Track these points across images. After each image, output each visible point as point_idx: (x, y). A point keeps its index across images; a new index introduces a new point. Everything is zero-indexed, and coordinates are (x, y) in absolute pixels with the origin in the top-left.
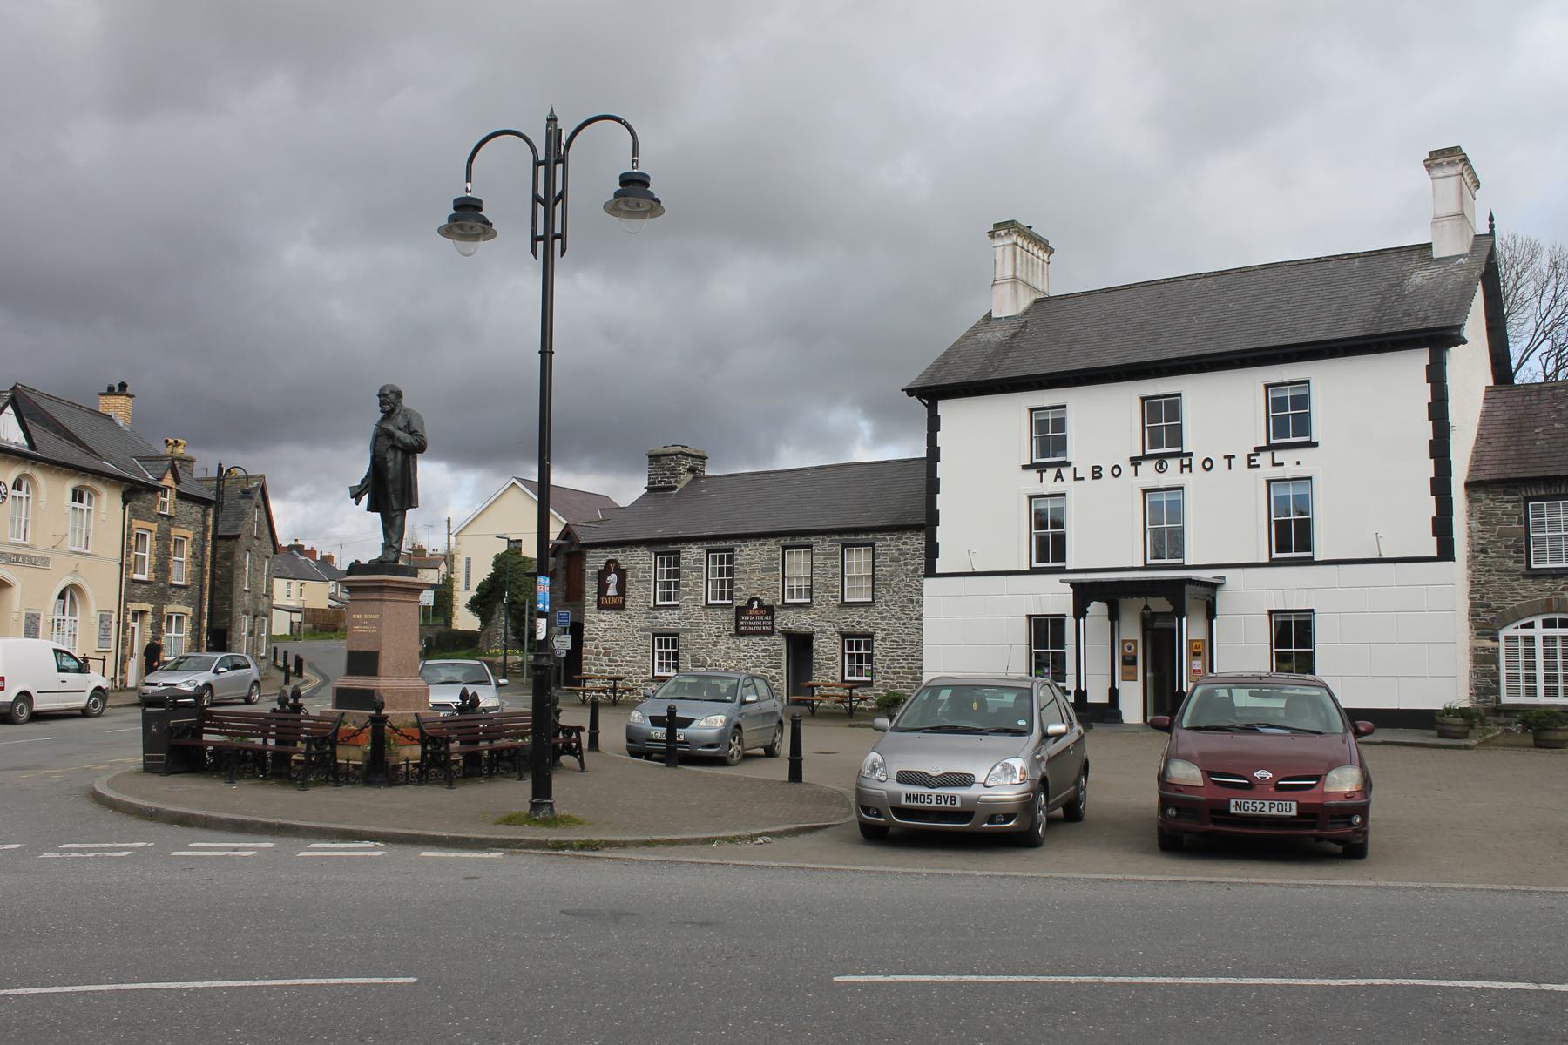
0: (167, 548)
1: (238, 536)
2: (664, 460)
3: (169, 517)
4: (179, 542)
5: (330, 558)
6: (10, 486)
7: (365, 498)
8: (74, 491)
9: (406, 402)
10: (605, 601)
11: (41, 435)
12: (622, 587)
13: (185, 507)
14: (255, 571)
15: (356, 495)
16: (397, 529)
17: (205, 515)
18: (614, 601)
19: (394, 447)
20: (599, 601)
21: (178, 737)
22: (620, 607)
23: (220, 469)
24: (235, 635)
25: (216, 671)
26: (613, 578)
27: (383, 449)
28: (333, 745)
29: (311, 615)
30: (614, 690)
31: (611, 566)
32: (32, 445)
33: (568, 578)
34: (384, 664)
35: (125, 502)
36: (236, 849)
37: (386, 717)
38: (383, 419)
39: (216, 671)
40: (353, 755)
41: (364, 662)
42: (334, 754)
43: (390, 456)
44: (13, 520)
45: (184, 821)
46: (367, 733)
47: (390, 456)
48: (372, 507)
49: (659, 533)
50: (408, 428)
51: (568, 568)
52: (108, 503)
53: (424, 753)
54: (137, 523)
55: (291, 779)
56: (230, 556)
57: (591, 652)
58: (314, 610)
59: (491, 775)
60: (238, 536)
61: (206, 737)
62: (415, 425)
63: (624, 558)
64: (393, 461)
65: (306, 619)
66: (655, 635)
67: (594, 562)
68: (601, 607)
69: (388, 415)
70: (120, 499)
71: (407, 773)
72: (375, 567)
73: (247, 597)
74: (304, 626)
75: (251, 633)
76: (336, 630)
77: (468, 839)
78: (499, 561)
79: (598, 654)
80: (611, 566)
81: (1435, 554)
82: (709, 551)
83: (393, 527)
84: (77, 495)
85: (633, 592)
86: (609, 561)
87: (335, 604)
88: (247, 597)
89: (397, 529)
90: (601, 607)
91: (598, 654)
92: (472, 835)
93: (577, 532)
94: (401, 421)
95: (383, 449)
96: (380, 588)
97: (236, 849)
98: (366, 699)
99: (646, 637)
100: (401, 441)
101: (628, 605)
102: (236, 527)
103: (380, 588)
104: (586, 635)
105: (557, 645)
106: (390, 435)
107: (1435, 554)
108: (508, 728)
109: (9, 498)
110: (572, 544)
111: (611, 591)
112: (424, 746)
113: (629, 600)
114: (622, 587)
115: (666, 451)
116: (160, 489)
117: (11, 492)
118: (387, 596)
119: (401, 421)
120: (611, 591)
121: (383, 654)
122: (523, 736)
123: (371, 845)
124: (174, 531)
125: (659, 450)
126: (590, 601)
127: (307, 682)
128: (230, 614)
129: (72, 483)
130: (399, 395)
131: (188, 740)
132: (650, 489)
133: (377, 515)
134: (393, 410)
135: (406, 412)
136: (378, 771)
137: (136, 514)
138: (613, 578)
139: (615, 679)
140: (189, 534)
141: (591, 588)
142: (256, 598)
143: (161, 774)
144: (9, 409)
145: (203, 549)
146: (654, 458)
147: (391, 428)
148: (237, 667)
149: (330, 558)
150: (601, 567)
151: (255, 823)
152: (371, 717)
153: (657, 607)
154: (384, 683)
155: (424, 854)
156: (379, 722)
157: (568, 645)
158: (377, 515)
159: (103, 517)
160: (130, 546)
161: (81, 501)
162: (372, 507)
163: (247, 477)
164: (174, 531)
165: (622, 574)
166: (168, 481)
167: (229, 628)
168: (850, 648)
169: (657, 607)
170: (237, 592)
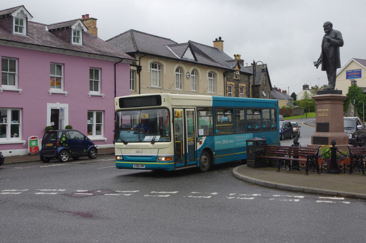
0: (238, 90)
3: (238, 80)
4: (242, 89)
6: (191, 73)
7: (320, 66)
8: (209, 73)
9: (334, 28)
11: (198, 57)
13: (243, 76)
17: (249, 79)
32: (196, 60)
34: (331, 127)
35: (224, 76)
38: (326, 35)
44: (192, 84)
45: (276, 188)
48: (323, 69)
52: (220, 77)
54: (228, 83)
60: (260, 85)
70: (223, 75)
71: (322, 168)
72: (326, 90)
78: (350, 89)
81: (185, 109)
83: (332, 77)
84: (210, 75)
94: (332, 35)
107: (185, 109)
109: (191, 77)
116: (235, 71)
117: (191, 75)
119: (332, 35)
122: (199, 154)
124: (240, 85)
129: (208, 71)
130: (265, 71)
137: (228, 80)
140: (244, 85)
144: (189, 49)
145: (249, 90)
152: (331, 148)
155: (319, 197)
159: (218, 81)
160: (227, 91)
161: (211, 77)
162: (323, 69)
163: (263, 65)
164: (240, 85)
166: (237, 68)
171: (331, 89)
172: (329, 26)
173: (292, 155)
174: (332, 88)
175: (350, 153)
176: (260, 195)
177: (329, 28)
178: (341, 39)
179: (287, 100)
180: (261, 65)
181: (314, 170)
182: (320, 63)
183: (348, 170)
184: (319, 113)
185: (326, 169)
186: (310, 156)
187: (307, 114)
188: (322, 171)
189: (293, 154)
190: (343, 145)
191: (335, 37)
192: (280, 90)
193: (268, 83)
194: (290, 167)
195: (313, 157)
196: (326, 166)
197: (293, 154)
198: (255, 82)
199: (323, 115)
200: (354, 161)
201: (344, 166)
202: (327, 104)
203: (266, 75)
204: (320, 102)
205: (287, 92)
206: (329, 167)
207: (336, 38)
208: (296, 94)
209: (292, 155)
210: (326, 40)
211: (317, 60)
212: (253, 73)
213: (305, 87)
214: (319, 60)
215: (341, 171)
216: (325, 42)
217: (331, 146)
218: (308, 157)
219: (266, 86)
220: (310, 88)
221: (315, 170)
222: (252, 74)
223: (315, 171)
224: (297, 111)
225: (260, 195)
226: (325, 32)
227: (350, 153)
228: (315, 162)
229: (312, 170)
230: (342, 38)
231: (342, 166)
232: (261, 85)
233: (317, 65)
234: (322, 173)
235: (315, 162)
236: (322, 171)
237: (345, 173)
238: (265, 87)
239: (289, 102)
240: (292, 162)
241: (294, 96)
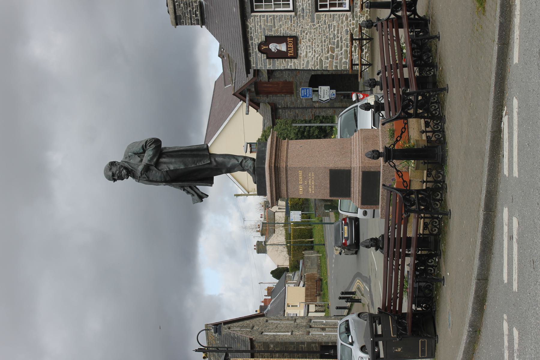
1: (251, 339)
2: (179, 13)
5: (269, 289)
7: (202, 188)
9: (119, 158)
10: (291, 53)
12: (280, 39)
14: (277, 328)
15: (202, 197)
16: (226, 160)
18: (291, 45)
19: (157, 164)
20: (291, 58)
21: (405, 329)
22: (295, 40)
23: (199, 350)
24: (325, 340)
25: (352, 344)
26: (273, 47)
27: (159, 174)
28: (411, 192)
29: (310, 297)
30: (361, 40)
31: (263, 49)
33: (275, 93)
34: (340, 164)
36: (511, 238)
37: (386, 148)
38: (134, 177)
39: (352, 344)
40: (417, 177)
41: (339, 181)
42: (418, 192)
43: (164, 168)
45: (483, 280)
46: (400, 164)
47: (164, 168)
49: (236, 10)
50: (140, 154)
51: (267, 94)
53: (417, 116)
55: (439, 233)
56: (266, 344)
57: (331, 62)
58: (307, 296)
59: (433, 66)
60: (251, 339)
61: (405, 310)
62: (138, 149)
63: (256, 39)
64: (171, 165)
65: (313, 301)
66: (317, 11)
67: (260, 62)
68: (295, 56)
69: (130, 173)
71: (433, 132)
72: (258, 174)
73: (296, 333)
74: (318, 302)
75: (323, 329)
76: (321, 280)
77: (501, 24)
79: (332, 57)
80: (263, 49)
82: (253, 11)
85: (283, 30)
86: (260, 50)
87: (302, 284)
88: (296, 333)
89: (226, 160)
90: (295, 56)
91: (332, 57)
92: (497, 24)
93: (238, 87)
95: (159, 174)
96: (276, 170)
97: (511, 238)
98: (370, 179)
99: (319, 18)
100: (152, 159)
101: (294, 34)
102: (244, 341)
103: (276, 170)
104: (318, 67)
105: (327, 98)
106: (147, 168)
108: (394, 60)
110: (249, 90)
111: (283, 47)
112: (410, 116)
113: (289, 33)
114: (280, 39)
115: (171, 11)
118: (283, 165)
120: (283, 47)
121: (332, 166)
123: (505, 119)
125: (169, 18)
126: (291, 64)
127: (359, 288)
128: (309, 344)
130: (112, 164)
131: (408, 322)
132: (203, 22)
133: (216, 178)
134: (126, 168)
135: (128, 156)
136: (432, 155)
138: (273, 47)
139: (352, 39)
141: (280, 64)
142: (297, 327)
143: (436, 342)
146: (178, 21)
147: (140, 168)
148: (348, 330)
149: (269, 289)
150: (264, 56)
151: (483, 232)
152: (386, 161)
153: (294, 10)
154: (357, 163)
155: (516, 60)
156: (390, 154)
157: (327, 88)
158: (216, 178)
162: (209, 181)
165: (269, 39)
167: (320, 343)
168: (325, 6)
169: (294, 10)
170: (293, 339)
171: (254, 164)
172: (114, 169)
173: (404, 251)
174: (252, 162)
175: (397, 119)
176: (505, 317)
177: (120, 168)
178: (144, 143)
179: (286, 285)
180: (207, 334)
181: (438, 200)
182: (196, 190)
183: (438, 124)
184: (308, 191)
185: (434, 173)
186: (405, 206)
187: (316, 245)
188: (440, 182)
189: (394, 89)
190: (381, 139)
191: (139, 156)
192: (265, 301)
193: (248, 322)
194: (430, 256)
195: (409, 200)
196: (427, 171)
197: (394, 89)
198: (244, 348)
199: (312, 183)
200: (417, 111)
201: (428, 134)
202: (286, 174)
203: (229, 325)
204: (283, 188)
205: (271, 285)
206: (430, 166)
207: (141, 153)
208: (274, 268)
209: (404, 251)
210: (144, 176)
211: (190, 196)
212: (225, 354)
213: (261, 248)
214: (188, 193)
215: (438, 139)
216: (148, 178)
217: (381, 159)
218: (408, 211)
219: (253, 327)
220: (262, 239)
221: (438, 197)
222: (227, 355)
223: (441, 197)
224: (311, 264)
225: (505, 317)
226: (127, 178)
227: (397, 119)
228: (420, 196)
229: (437, 203)
230: (141, 142)
231: (427, 137)
232: (251, 337)
233: (202, 197)
234: (444, 182)
235: (420, 196)
236: (440, 182)
237: (442, 131)
238: (255, 328)
239: (291, 283)
240: (421, 250)
241: (278, 273)
